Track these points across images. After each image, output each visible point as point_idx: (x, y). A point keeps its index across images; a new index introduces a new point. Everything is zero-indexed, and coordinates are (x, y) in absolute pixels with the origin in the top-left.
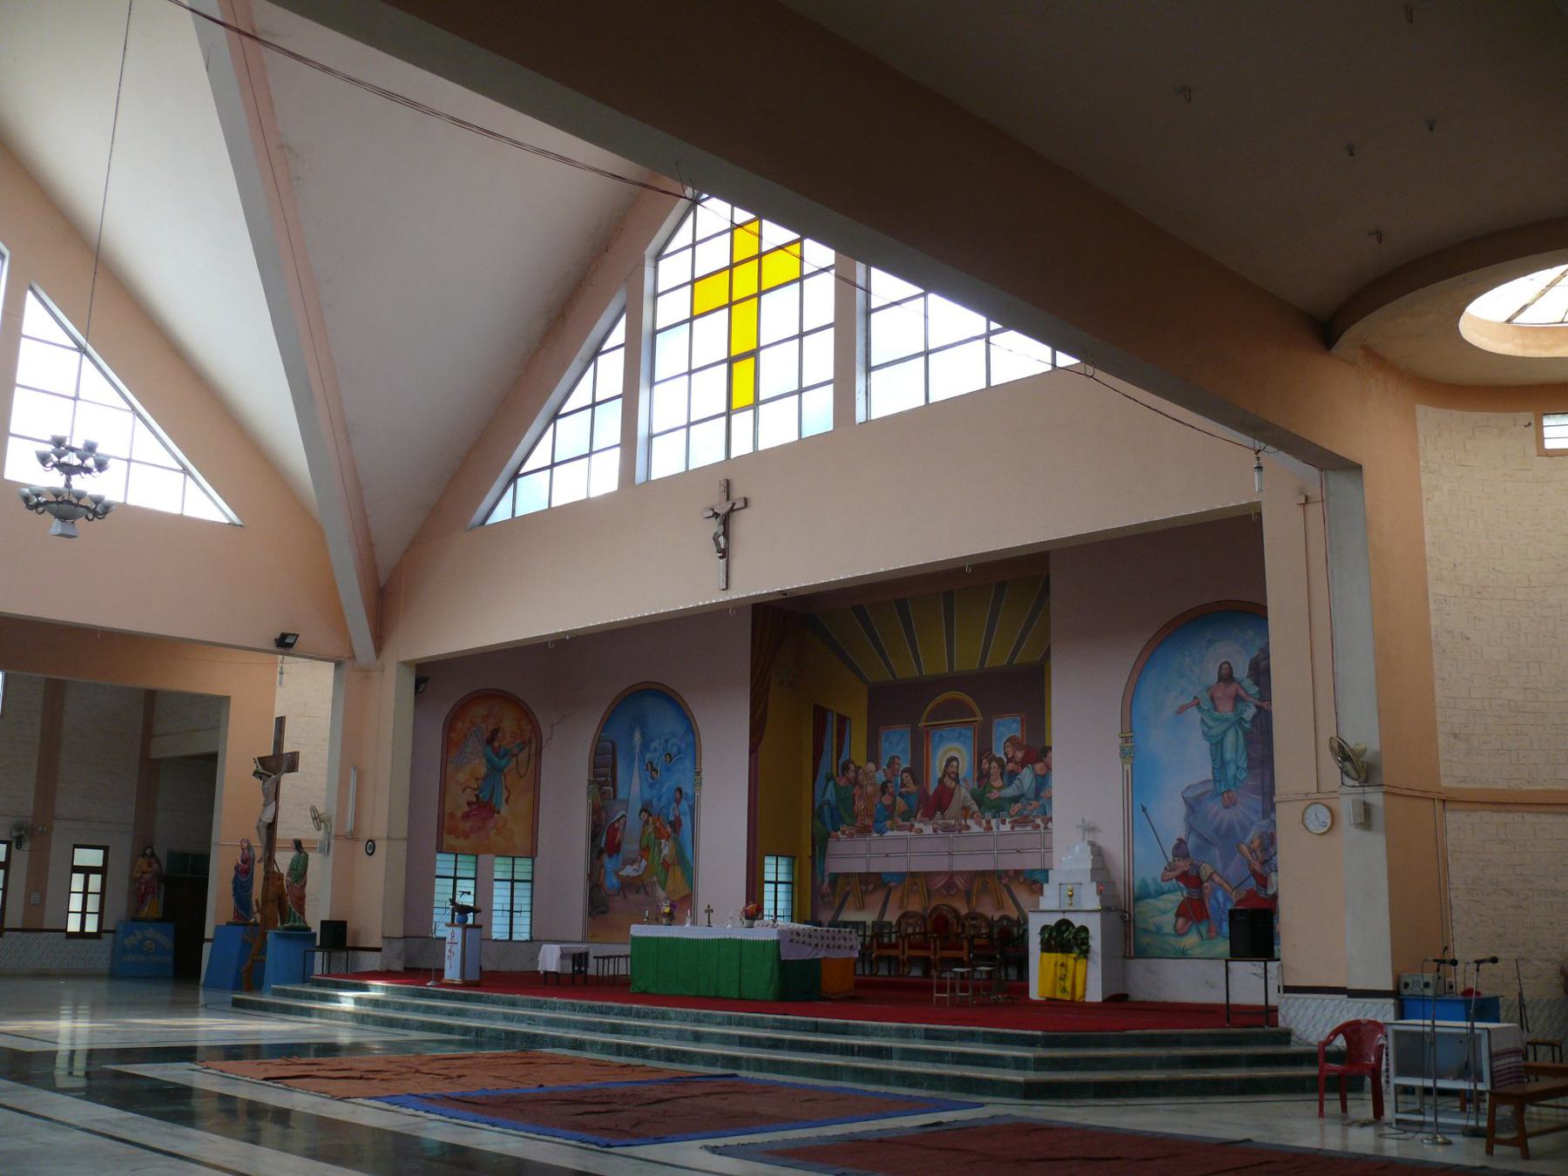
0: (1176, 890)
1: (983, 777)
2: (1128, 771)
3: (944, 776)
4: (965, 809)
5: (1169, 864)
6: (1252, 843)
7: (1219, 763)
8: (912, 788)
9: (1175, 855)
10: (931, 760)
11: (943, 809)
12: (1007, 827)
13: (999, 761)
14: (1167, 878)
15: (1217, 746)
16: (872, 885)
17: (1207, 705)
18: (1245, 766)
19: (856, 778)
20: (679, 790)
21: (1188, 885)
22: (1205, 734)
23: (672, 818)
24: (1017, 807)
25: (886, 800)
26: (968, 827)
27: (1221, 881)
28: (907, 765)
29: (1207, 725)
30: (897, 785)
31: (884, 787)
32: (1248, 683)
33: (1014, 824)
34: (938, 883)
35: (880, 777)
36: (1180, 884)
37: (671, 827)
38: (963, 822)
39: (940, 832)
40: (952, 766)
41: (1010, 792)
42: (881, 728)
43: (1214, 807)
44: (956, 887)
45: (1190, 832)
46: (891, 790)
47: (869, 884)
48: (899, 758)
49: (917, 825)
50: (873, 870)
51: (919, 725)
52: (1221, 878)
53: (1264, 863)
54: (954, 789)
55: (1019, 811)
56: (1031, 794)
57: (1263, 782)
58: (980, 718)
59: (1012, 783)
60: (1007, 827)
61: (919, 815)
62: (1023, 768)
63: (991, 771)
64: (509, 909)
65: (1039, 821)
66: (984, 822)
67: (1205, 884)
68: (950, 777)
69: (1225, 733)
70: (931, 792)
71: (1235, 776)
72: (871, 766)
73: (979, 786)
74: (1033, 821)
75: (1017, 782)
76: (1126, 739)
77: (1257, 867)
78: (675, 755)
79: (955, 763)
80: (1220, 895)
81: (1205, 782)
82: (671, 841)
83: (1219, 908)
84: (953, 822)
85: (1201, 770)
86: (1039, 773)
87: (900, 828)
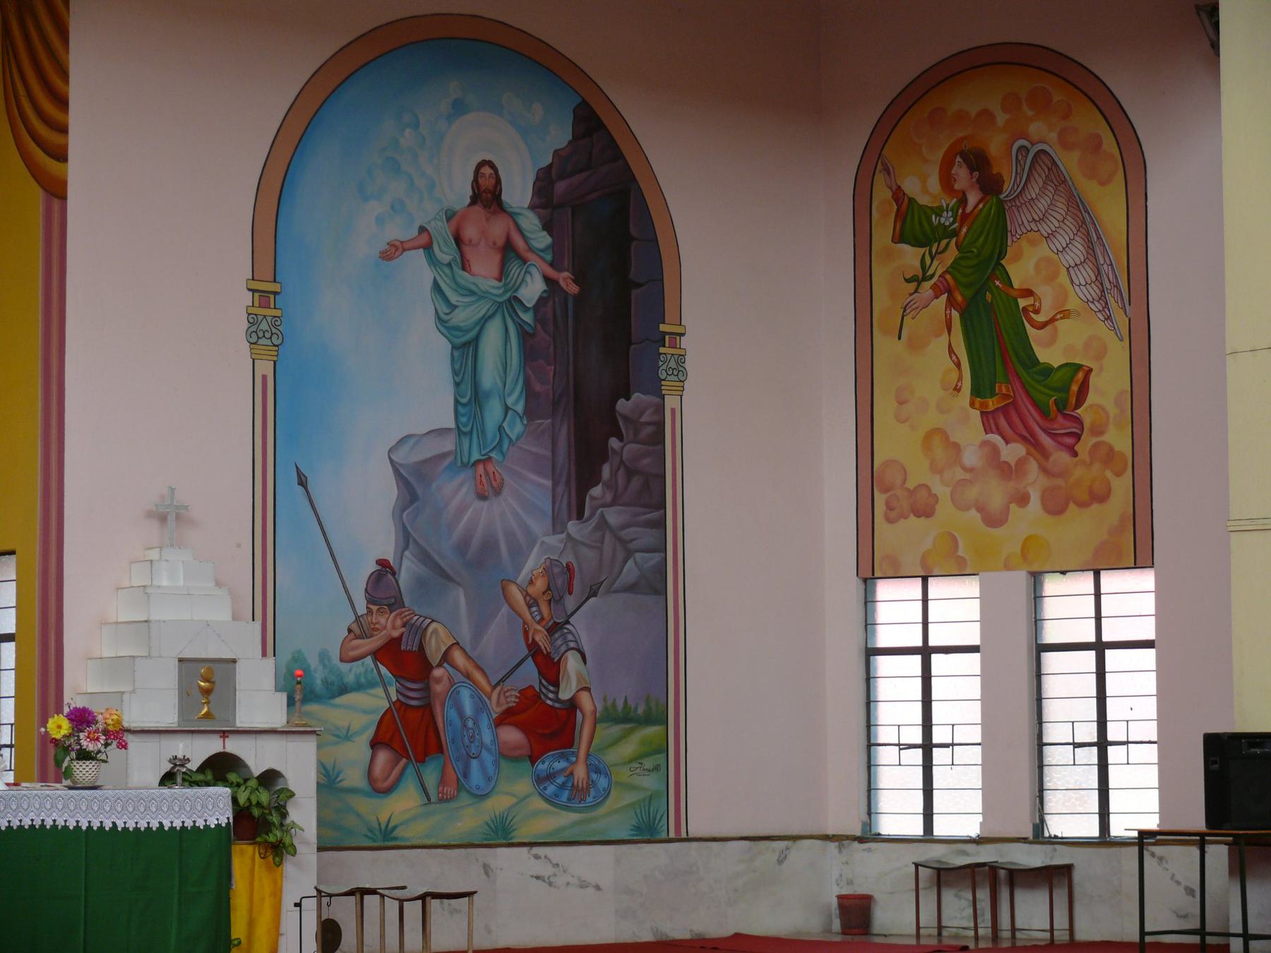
0: (372, 685)
2: (264, 378)
6: (531, 582)
9: (371, 600)
17: (446, 253)
18: (520, 408)
21: (399, 673)
22: (440, 320)
32: (530, 222)
36: (383, 670)
52: (469, 657)
53: (553, 628)
64: (918, 740)
67: (437, 673)
69: (485, 320)
71: (500, 428)
76: (264, 298)
77: (541, 639)
81: (441, 432)
83: (465, 726)
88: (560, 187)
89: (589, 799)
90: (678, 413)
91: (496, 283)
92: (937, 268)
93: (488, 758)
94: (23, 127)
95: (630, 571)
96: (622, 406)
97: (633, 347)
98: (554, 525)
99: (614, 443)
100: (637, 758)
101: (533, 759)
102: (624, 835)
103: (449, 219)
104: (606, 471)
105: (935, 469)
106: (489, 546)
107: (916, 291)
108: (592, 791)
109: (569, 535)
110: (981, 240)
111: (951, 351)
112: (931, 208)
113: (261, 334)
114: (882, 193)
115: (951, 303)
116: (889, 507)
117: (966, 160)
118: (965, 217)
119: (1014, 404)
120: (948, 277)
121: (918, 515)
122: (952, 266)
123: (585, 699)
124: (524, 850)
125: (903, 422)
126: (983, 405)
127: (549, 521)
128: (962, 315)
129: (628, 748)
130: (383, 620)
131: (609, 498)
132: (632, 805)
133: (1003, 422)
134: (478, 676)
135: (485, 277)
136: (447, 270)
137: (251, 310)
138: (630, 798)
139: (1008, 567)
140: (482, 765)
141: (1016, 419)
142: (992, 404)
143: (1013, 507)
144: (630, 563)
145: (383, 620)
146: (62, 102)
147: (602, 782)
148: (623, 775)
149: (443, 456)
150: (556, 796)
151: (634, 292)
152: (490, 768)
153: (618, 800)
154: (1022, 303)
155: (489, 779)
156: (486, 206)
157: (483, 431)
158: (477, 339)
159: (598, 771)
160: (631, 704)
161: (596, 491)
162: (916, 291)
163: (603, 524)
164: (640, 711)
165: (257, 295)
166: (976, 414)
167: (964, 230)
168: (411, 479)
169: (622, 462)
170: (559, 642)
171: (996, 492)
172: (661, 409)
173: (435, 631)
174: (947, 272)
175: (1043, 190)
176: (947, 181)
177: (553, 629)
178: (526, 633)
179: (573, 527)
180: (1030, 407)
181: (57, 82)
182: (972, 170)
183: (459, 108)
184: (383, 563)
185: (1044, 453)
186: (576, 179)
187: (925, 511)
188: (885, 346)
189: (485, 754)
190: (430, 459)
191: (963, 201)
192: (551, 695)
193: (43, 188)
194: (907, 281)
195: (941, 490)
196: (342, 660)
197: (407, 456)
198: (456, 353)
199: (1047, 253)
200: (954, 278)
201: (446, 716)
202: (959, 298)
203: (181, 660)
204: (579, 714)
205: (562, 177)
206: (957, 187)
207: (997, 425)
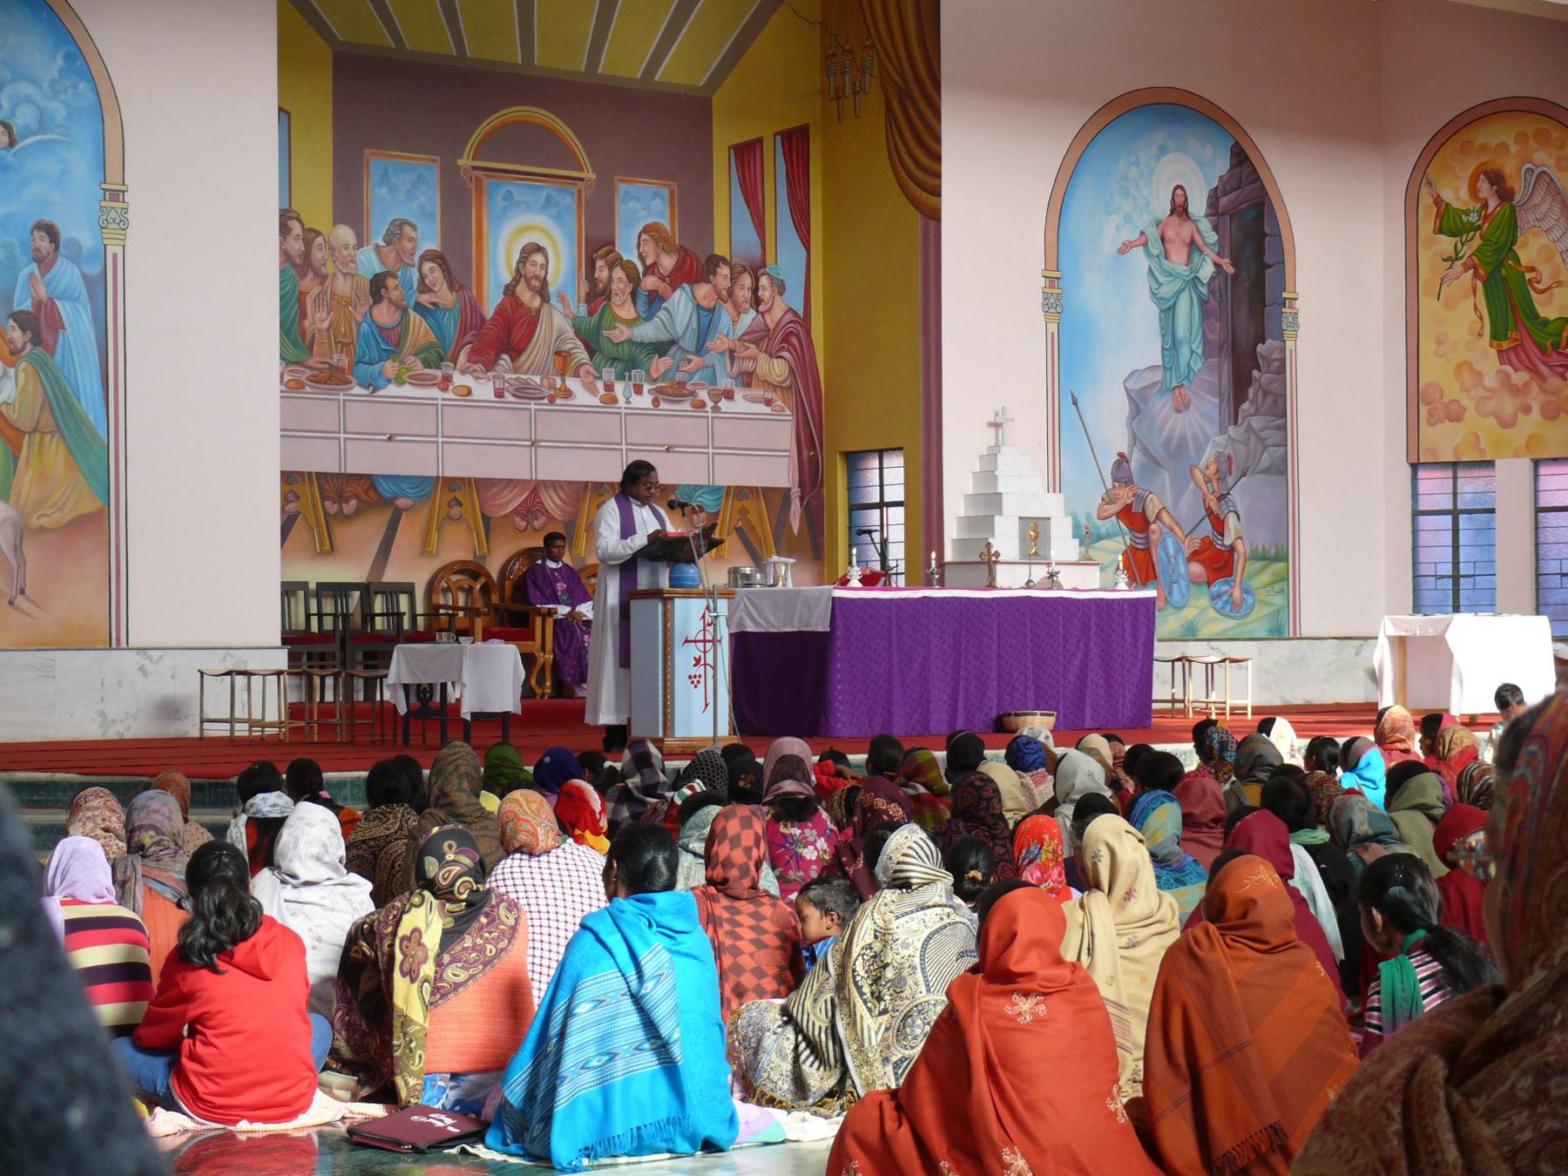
0: (1115, 535)
1: (597, 295)
2: (1053, 334)
3: (516, 281)
4: (563, 356)
5: (1107, 491)
6: (1207, 467)
7: (1171, 346)
8: (445, 296)
9: (1115, 479)
10: (488, 243)
11: (516, 354)
12: (644, 401)
13: (628, 268)
14: (1104, 514)
15: (1168, 312)
16: (353, 502)
17: (1156, 248)
18: (1200, 351)
19: (307, 255)
20: (51, 232)
23: (23, 303)
24: (661, 364)
25: (385, 315)
26: (568, 394)
27: (1172, 524)
28: (432, 244)
29: (1157, 280)
30: (412, 287)
31: (377, 286)
32: (1205, 226)
33: (660, 395)
34: (508, 503)
35: (369, 263)
36: (1122, 524)
37: (23, 329)
38: (559, 384)
39: (508, 397)
40: (534, 264)
41: (649, 331)
42: (367, 151)
43: (1162, 406)
44: (545, 512)
45: (1134, 445)
46: (395, 294)
47: (347, 501)
48: (414, 228)
49: (459, 379)
50: (353, 469)
51: (460, 162)
52: (1171, 516)
53: (1221, 498)
54: (538, 311)
55: (667, 371)
56: (689, 342)
57: (1220, 379)
58: (589, 175)
59: (654, 315)
60: (644, 401)
61: (463, 357)
62: (674, 291)
63: (614, 286)
65: (703, 395)
66: (600, 385)
67: (1153, 527)
68: (528, 281)
70: (489, 311)
71: (1189, 365)
72: (345, 234)
73: (591, 313)
74: (693, 394)
75: (662, 314)
76: (1052, 281)
77: (1214, 505)
78: (29, 133)
79: (539, 258)
80: (1170, 542)
81: (1153, 368)
82: (23, 365)
83: (1169, 562)
84: (537, 379)
85: (1149, 352)
86: (704, 304)
87: (419, 381)
88: (1223, 201)
89: (1242, 611)
90: (1294, 352)
91: (1185, 268)
92: (1466, 251)
93: (1183, 583)
94: (902, 171)
95: (1266, 460)
96: (1260, 348)
97: (1267, 308)
98: (1220, 430)
99: (1255, 373)
100: (1271, 584)
101: (1209, 584)
102: (1263, 635)
103: (1157, 225)
104: (1251, 391)
105: (1464, 389)
106: (1182, 443)
107: (1450, 268)
108: (1244, 606)
109: (1229, 436)
110: (1498, 232)
111: (1476, 309)
112: (1462, 210)
113: (111, 221)
114: (1426, 200)
115: (1476, 276)
116: (1431, 415)
117: (1488, 177)
118: (1486, 217)
119: (1522, 345)
120: (1474, 258)
121: (1451, 420)
122: (1477, 250)
123: (1240, 546)
124: (1206, 643)
125: (1440, 357)
126: (1498, 346)
127: (1217, 428)
128: (1484, 284)
129: (1265, 577)
130: (1121, 492)
131: (1252, 410)
132: (1267, 615)
133: (1513, 357)
134: (1176, 529)
135: (1179, 264)
136: (1156, 260)
137: (1046, 290)
138: (1267, 610)
139: (1516, 455)
140: (1179, 587)
141: (1523, 356)
142: (1505, 345)
143: (1520, 415)
144: (1266, 454)
145: (1121, 492)
146: (937, 158)
147: (1250, 600)
148: (1262, 595)
149: (1155, 384)
150: (1223, 608)
151: (1267, 271)
152: (1184, 590)
153: (1259, 612)
154: (1528, 276)
155: (1184, 597)
156: (1179, 216)
157: (1179, 367)
158: (1174, 305)
159: (1247, 592)
160: (1267, 547)
161: (1245, 406)
162: (1450, 268)
163: (1250, 428)
164: (1272, 552)
165: (107, 193)
166: (1494, 352)
167: (1486, 225)
168: (1136, 399)
169: (1260, 386)
170: (1224, 507)
171: (1508, 405)
172: (1283, 350)
173: (1152, 499)
174: (1473, 254)
175: (1543, 199)
176: (1474, 192)
177: (1221, 498)
178: (1204, 501)
179: (1231, 430)
180: (1534, 348)
181: (933, 145)
182: (1492, 184)
183: (1163, 151)
184: (1121, 455)
185: (1543, 379)
186: (1233, 195)
187: (1456, 417)
188: (1428, 305)
189: (1181, 581)
190: (1148, 386)
191: (1485, 206)
192: (1219, 542)
193: (921, 212)
194: (1444, 260)
195: (1467, 402)
196: (1099, 518)
197: (1135, 385)
198: (1163, 315)
199: (1547, 242)
200: (1479, 258)
201: (1158, 555)
202: (1482, 272)
203: (1020, 518)
204: (1236, 556)
205: (1225, 194)
206: (1481, 195)
207: (1509, 360)
